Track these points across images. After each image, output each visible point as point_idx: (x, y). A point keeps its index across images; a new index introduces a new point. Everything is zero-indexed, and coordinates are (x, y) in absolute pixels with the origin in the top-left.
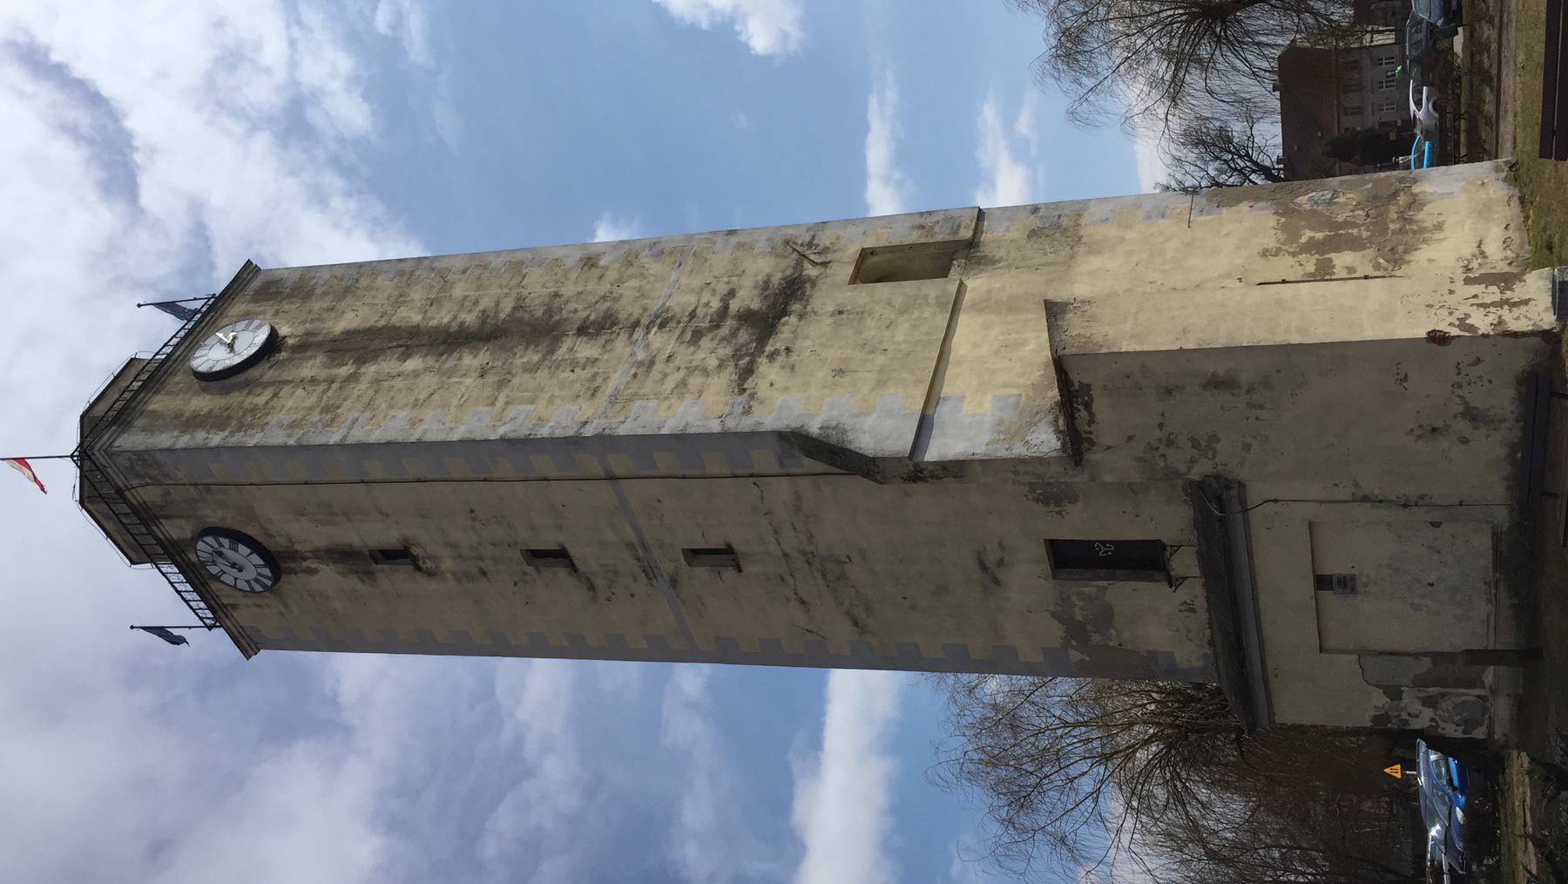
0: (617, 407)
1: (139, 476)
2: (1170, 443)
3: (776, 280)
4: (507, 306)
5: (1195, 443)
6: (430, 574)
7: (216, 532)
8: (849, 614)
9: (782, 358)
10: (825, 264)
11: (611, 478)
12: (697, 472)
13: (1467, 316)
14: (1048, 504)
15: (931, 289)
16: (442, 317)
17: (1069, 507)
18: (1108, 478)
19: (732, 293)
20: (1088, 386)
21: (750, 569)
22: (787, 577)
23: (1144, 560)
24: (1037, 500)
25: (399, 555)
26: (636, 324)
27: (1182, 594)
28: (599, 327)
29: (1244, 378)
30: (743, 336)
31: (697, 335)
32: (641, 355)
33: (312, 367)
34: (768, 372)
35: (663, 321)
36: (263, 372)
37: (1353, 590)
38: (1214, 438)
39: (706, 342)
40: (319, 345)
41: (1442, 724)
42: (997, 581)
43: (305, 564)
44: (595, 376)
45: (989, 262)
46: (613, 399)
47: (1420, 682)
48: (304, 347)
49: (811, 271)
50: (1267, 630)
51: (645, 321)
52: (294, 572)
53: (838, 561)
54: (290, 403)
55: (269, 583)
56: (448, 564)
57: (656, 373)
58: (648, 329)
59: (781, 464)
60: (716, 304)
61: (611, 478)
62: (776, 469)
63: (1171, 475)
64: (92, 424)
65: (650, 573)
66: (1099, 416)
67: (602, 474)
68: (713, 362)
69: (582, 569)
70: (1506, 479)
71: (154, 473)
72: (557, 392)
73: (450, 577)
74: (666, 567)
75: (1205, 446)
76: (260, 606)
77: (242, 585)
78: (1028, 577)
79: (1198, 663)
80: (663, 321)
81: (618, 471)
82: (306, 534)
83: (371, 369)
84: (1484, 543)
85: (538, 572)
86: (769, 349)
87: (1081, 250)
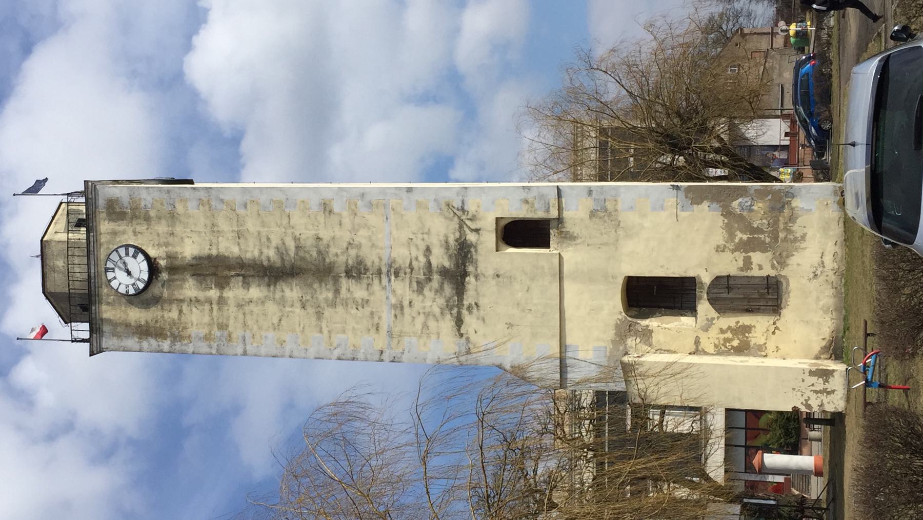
0: (395, 341)
28: (357, 271)
72: (356, 326)
87: (621, 232)
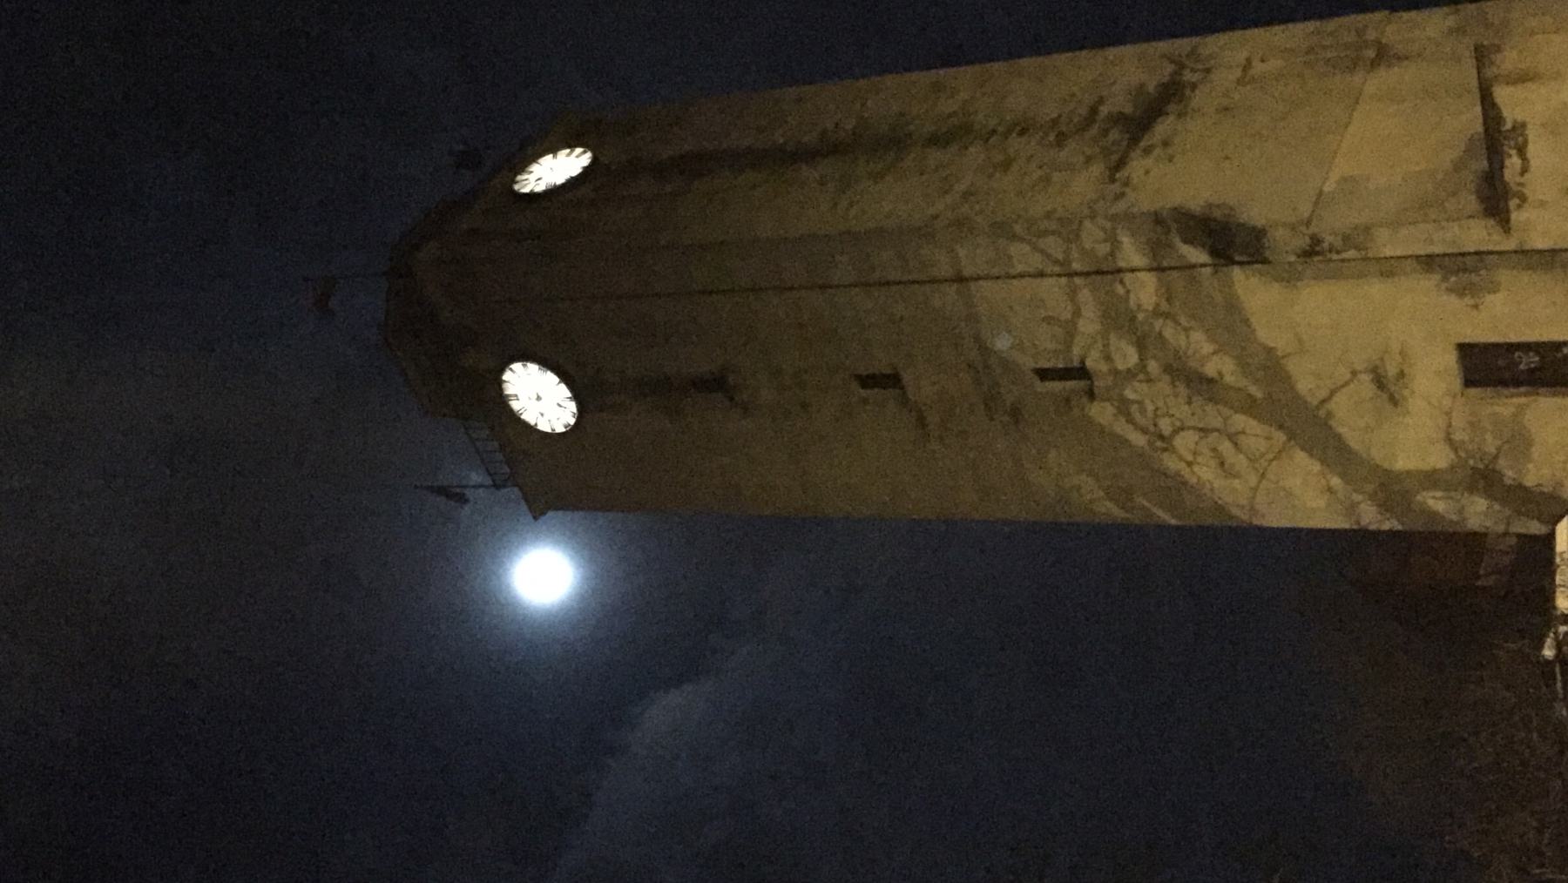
19: (1101, 101)
20: (1524, 125)
24: (1450, 290)
30: (1114, 135)
31: (1061, 139)
39: (1072, 144)
49: (1188, 76)
58: (1006, 135)
60: (1083, 111)
61: (960, 279)
66: (1534, 163)
86: (1142, 144)
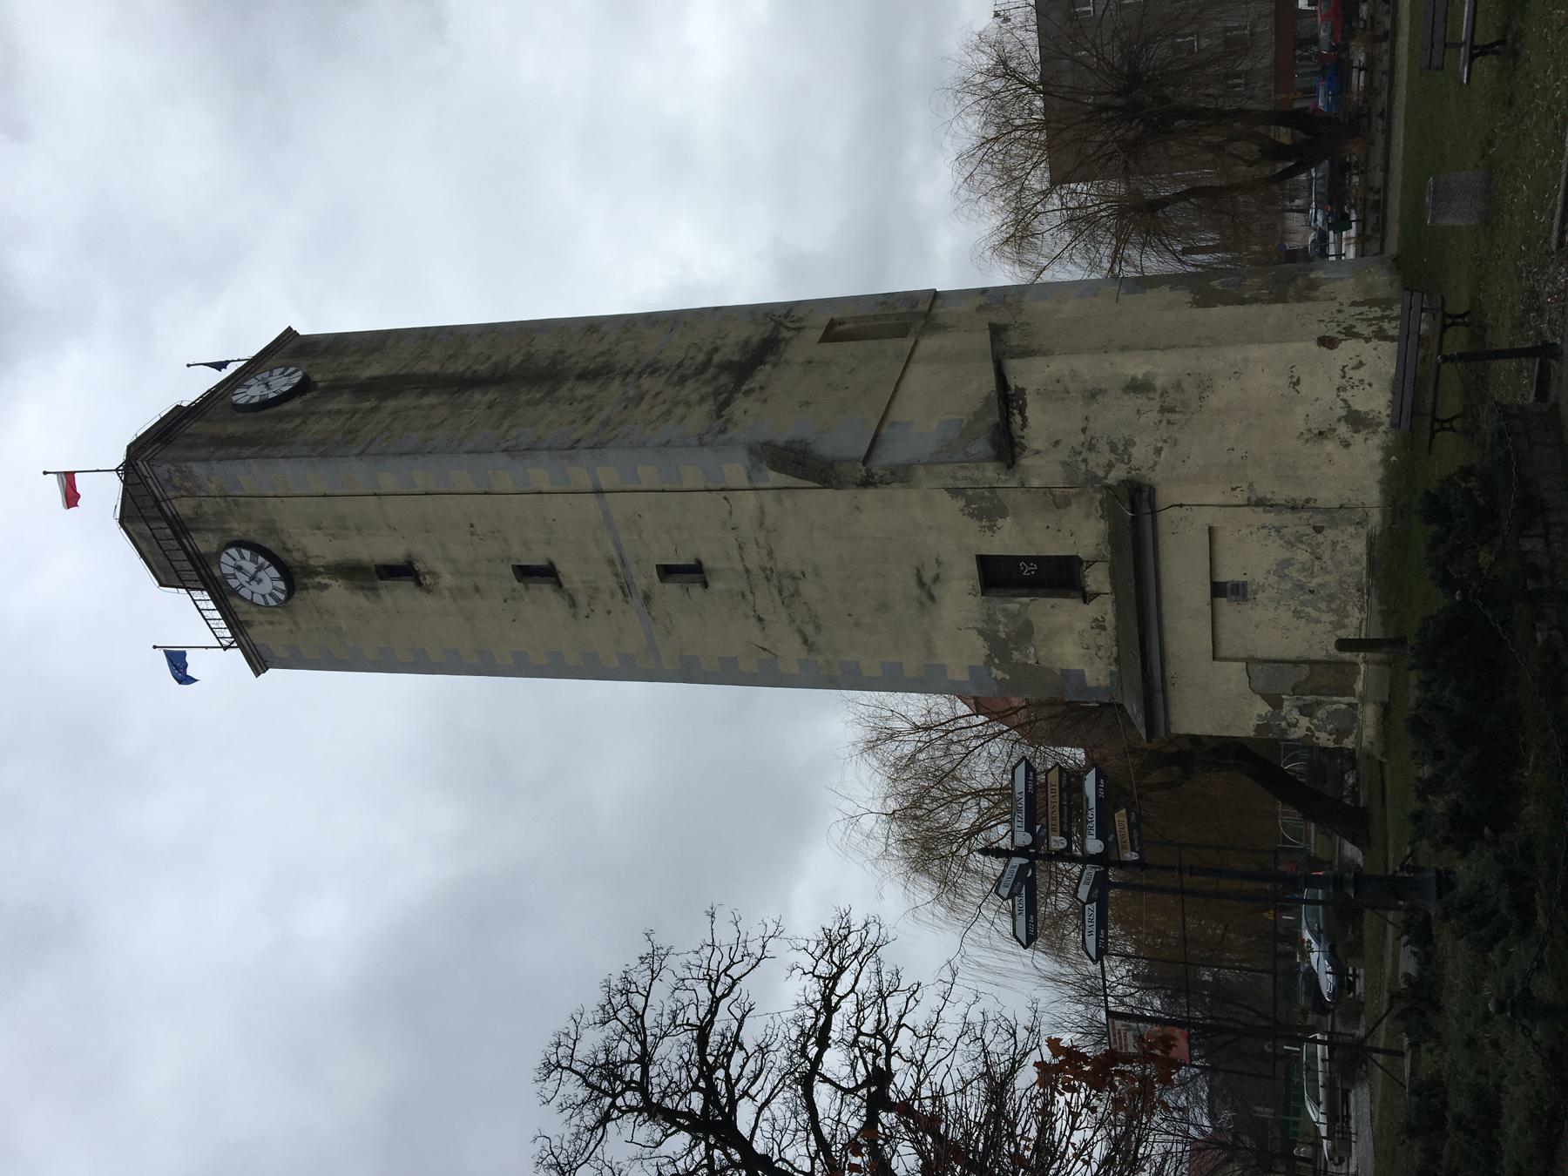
1: (176, 488)
2: (1091, 448)
3: (756, 339)
4: (517, 359)
5: (1113, 449)
6: (429, 590)
7: (240, 544)
8: (800, 631)
9: (756, 394)
10: (799, 329)
11: (598, 492)
12: (674, 487)
13: (1353, 327)
14: (981, 520)
15: (891, 345)
16: (460, 366)
17: (1000, 522)
18: (1036, 483)
19: (716, 350)
20: (1023, 390)
21: (716, 585)
22: (748, 594)
23: (1059, 576)
24: (971, 515)
25: (403, 571)
26: (628, 373)
27: (1091, 610)
29: (1159, 382)
31: (683, 380)
32: (632, 393)
33: (340, 403)
34: (741, 404)
35: (653, 369)
36: (295, 404)
37: (1244, 598)
38: (1129, 443)
39: (690, 384)
40: (348, 387)
41: (1317, 734)
42: (932, 598)
43: (318, 579)
44: (590, 408)
45: (942, 328)
46: (605, 424)
47: (1296, 690)
48: (335, 388)
50: (1169, 638)
51: (637, 370)
52: (306, 588)
53: (793, 578)
54: (316, 428)
55: (282, 597)
56: (447, 580)
57: (644, 406)
58: (640, 375)
59: (749, 478)
60: (701, 357)
61: (598, 492)
62: (746, 484)
63: (1092, 479)
64: (137, 450)
65: (626, 590)
67: (590, 487)
68: (695, 397)
69: (566, 586)
70: (1380, 482)
71: (189, 485)
73: (447, 593)
74: (641, 583)
75: (1121, 450)
76: (271, 623)
77: (258, 599)
78: (960, 596)
79: (1104, 681)
80: (653, 369)
81: (605, 485)
82: (320, 548)
83: (391, 404)
84: (1359, 548)
85: (527, 589)
86: (745, 388)
